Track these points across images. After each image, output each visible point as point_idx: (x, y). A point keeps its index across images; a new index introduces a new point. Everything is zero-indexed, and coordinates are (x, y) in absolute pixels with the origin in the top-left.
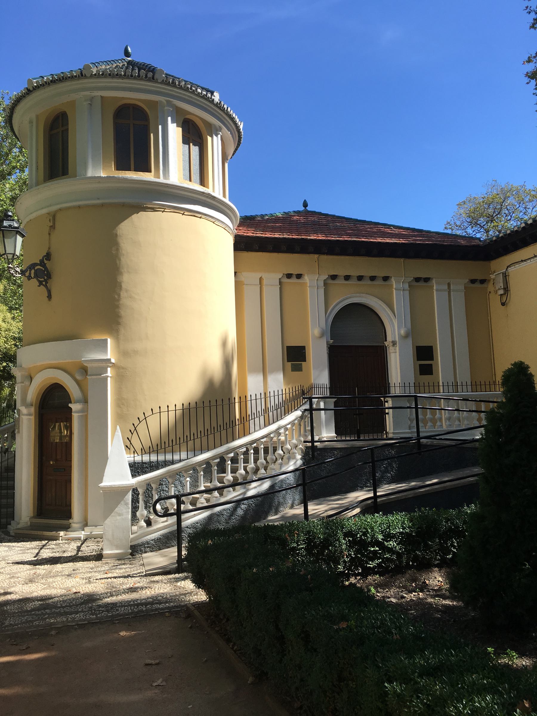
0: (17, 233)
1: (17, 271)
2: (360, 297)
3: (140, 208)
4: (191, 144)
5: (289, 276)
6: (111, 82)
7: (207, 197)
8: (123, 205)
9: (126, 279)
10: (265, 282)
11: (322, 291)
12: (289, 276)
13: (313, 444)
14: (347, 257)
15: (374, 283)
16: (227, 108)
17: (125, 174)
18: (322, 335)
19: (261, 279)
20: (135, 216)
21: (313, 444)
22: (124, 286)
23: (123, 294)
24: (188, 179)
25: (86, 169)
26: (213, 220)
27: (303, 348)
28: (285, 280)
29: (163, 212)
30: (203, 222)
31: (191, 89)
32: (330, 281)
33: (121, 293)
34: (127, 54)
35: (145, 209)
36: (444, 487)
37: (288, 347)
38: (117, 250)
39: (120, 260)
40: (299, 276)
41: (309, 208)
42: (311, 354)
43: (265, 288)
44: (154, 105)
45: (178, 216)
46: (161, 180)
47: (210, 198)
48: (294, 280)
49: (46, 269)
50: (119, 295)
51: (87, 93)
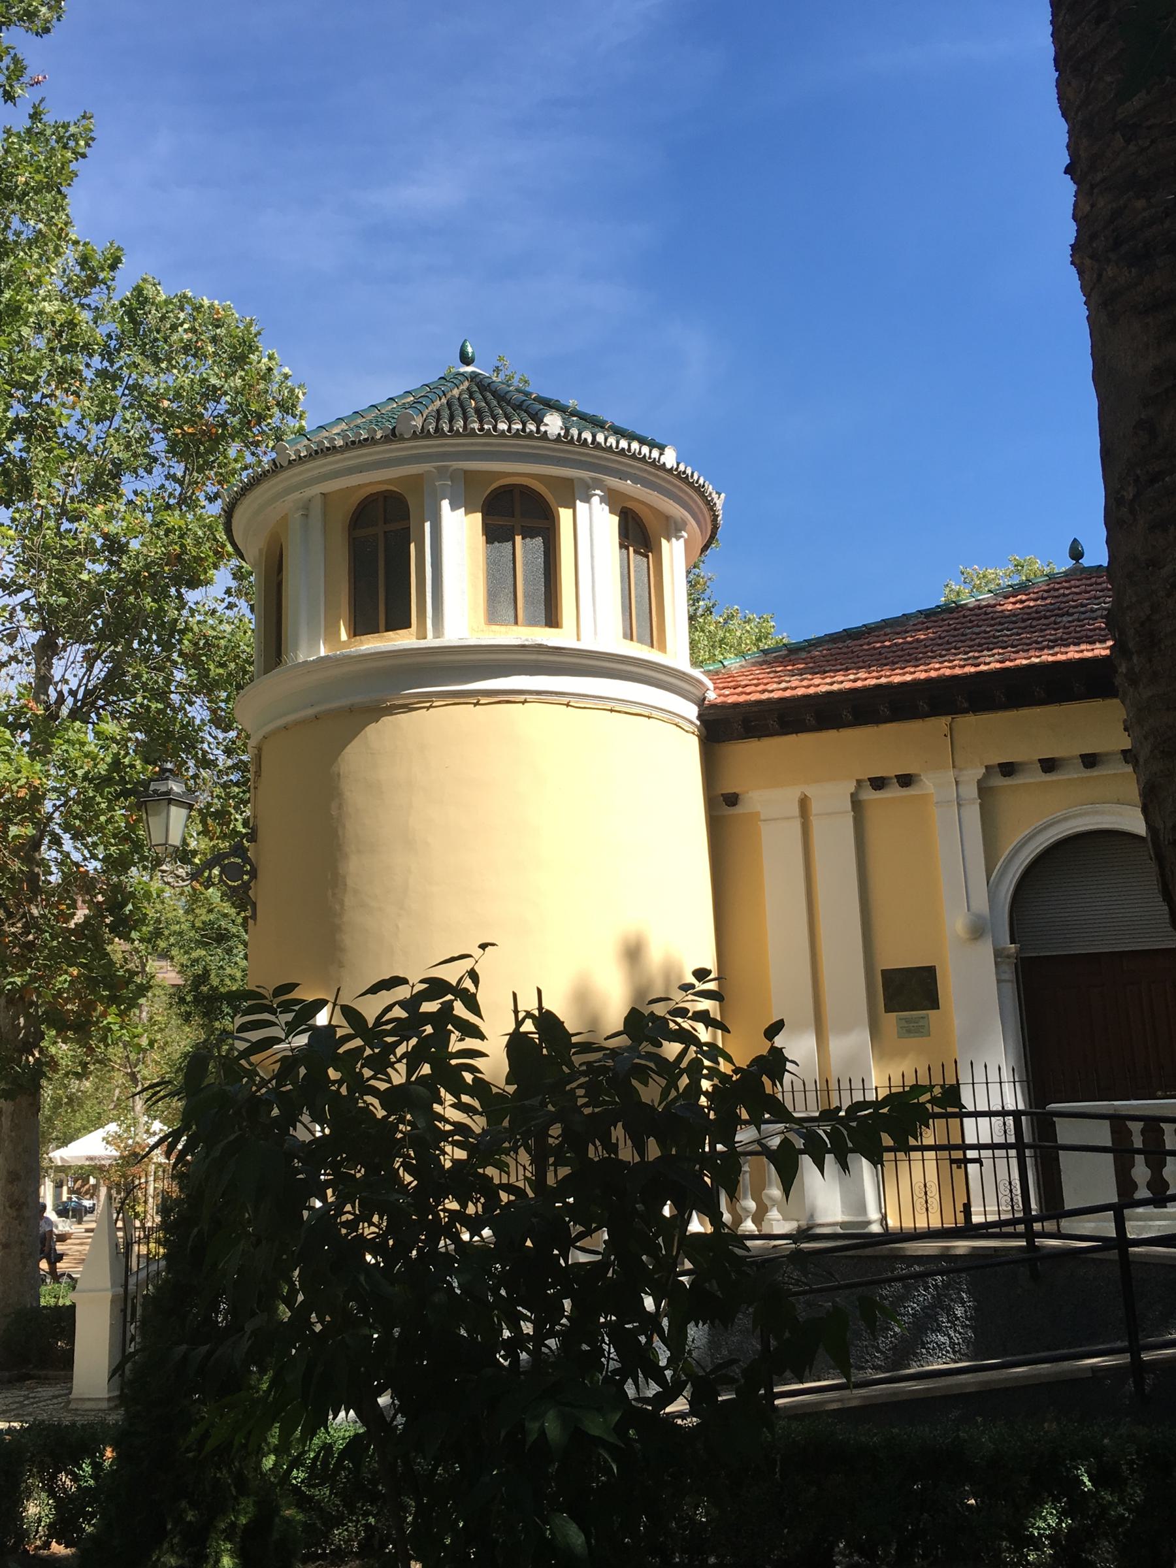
0: (169, 803)
1: (178, 877)
2: (1097, 813)
3: (377, 711)
4: (518, 539)
5: (878, 783)
6: (300, 473)
7: (539, 653)
8: (351, 710)
9: (353, 866)
10: (815, 808)
11: (973, 813)
12: (878, 783)
13: (1031, 1242)
14: (1038, 710)
15: (1094, 773)
16: (594, 437)
17: (362, 643)
18: (977, 931)
19: (804, 803)
20: (371, 729)
21: (1031, 1242)
22: (349, 882)
23: (349, 900)
24: (512, 620)
25: (296, 649)
26: (565, 700)
27: (930, 972)
28: (869, 795)
29: (428, 708)
30: (535, 711)
31: (482, 429)
32: (999, 781)
33: (346, 900)
34: (466, 359)
35: (391, 710)
36: (895, 1393)
37: (889, 976)
38: (340, 807)
39: (344, 827)
40: (906, 781)
41: (1086, 562)
42: (950, 986)
43: (816, 824)
44: (418, 479)
45: (465, 712)
46: (431, 641)
47: (544, 653)
48: (894, 792)
49: (247, 860)
50: (342, 903)
51: (296, 495)
